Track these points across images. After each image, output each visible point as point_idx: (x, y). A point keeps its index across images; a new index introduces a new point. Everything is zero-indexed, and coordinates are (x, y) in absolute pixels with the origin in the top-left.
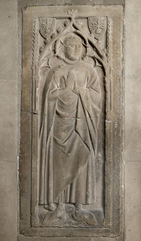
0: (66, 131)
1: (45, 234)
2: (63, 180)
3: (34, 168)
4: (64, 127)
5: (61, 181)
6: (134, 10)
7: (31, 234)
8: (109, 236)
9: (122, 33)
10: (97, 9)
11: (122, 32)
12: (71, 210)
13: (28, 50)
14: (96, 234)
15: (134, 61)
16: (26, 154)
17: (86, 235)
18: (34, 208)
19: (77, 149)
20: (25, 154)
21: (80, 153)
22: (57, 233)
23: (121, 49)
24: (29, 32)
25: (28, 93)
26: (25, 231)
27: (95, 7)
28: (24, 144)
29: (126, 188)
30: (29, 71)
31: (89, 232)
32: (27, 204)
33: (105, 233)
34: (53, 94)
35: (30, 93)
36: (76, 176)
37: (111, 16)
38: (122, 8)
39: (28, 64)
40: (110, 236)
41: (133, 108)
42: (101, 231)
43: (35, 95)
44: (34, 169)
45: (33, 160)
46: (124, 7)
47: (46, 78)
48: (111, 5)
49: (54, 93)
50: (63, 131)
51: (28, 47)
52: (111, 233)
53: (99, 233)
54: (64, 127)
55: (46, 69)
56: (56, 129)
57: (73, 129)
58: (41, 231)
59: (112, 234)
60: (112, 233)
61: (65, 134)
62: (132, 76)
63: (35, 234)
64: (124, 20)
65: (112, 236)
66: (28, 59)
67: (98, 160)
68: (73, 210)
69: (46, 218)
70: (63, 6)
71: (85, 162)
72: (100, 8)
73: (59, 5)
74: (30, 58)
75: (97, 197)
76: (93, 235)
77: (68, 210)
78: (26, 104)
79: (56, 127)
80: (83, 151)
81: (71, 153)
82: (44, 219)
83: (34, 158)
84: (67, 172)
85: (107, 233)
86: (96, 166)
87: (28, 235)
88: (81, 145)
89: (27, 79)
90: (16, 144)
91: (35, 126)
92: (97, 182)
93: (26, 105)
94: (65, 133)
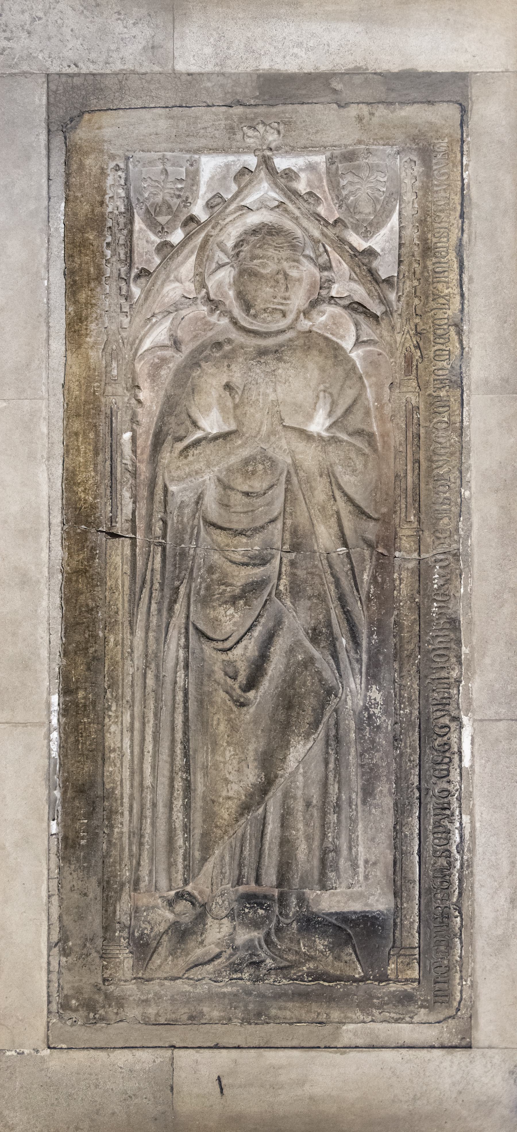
0: (242, 602)
1: (158, 1015)
2: (229, 798)
3: (114, 750)
4: (231, 585)
5: (221, 800)
6: (504, 123)
7: (102, 1012)
8: (412, 1018)
9: (458, 214)
10: (360, 119)
11: (459, 208)
12: (262, 917)
13: (89, 283)
14: (359, 1014)
15: (505, 322)
16: (81, 694)
17: (319, 1014)
18: (112, 908)
19: (286, 671)
20: (77, 694)
21: (294, 689)
22: (206, 1009)
23: (454, 276)
24: (93, 211)
25: (90, 454)
26: (78, 1000)
27: (353, 111)
28: (76, 653)
29: (478, 825)
30: (92, 367)
31: (333, 1004)
32: (85, 895)
33: (396, 1006)
34: (186, 457)
35: (469, 184)
36: (277, 781)
37: (414, 146)
38: (458, 116)
39: (88, 339)
40: (416, 1019)
41: (502, 507)
42: (378, 998)
43: (136, 1047)
44: (112, 755)
45: (110, 716)
46: (464, 110)
47: (162, 393)
48: (414, 103)
49: (191, 453)
50: (226, 602)
51: (89, 274)
52: (422, 1006)
53: (373, 1006)
54: (231, 585)
55: (164, 360)
56: (202, 592)
57: (270, 594)
58: (143, 1001)
59: (423, 1011)
60: (425, 1007)
61: (236, 615)
62: (497, 382)
63: (117, 1014)
64: (465, 162)
65: (425, 1019)
66: (87, 318)
67: (370, 717)
68: (268, 917)
69: (163, 950)
70: (224, 109)
71: (315, 724)
72: (372, 114)
73: (208, 106)
74: (95, 315)
75: (366, 862)
76: (350, 1015)
77: (250, 915)
78: (83, 495)
79: (203, 585)
80: (305, 682)
81: (258, 689)
82: (152, 956)
83: (114, 708)
84: (243, 763)
85: (403, 1005)
86: (360, 738)
87: (91, 1015)
88: (300, 657)
89: (83, 398)
90: (44, 653)
91: (117, 584)
92: (364, 802)
93: (80, 499)
94: (236, 609)
